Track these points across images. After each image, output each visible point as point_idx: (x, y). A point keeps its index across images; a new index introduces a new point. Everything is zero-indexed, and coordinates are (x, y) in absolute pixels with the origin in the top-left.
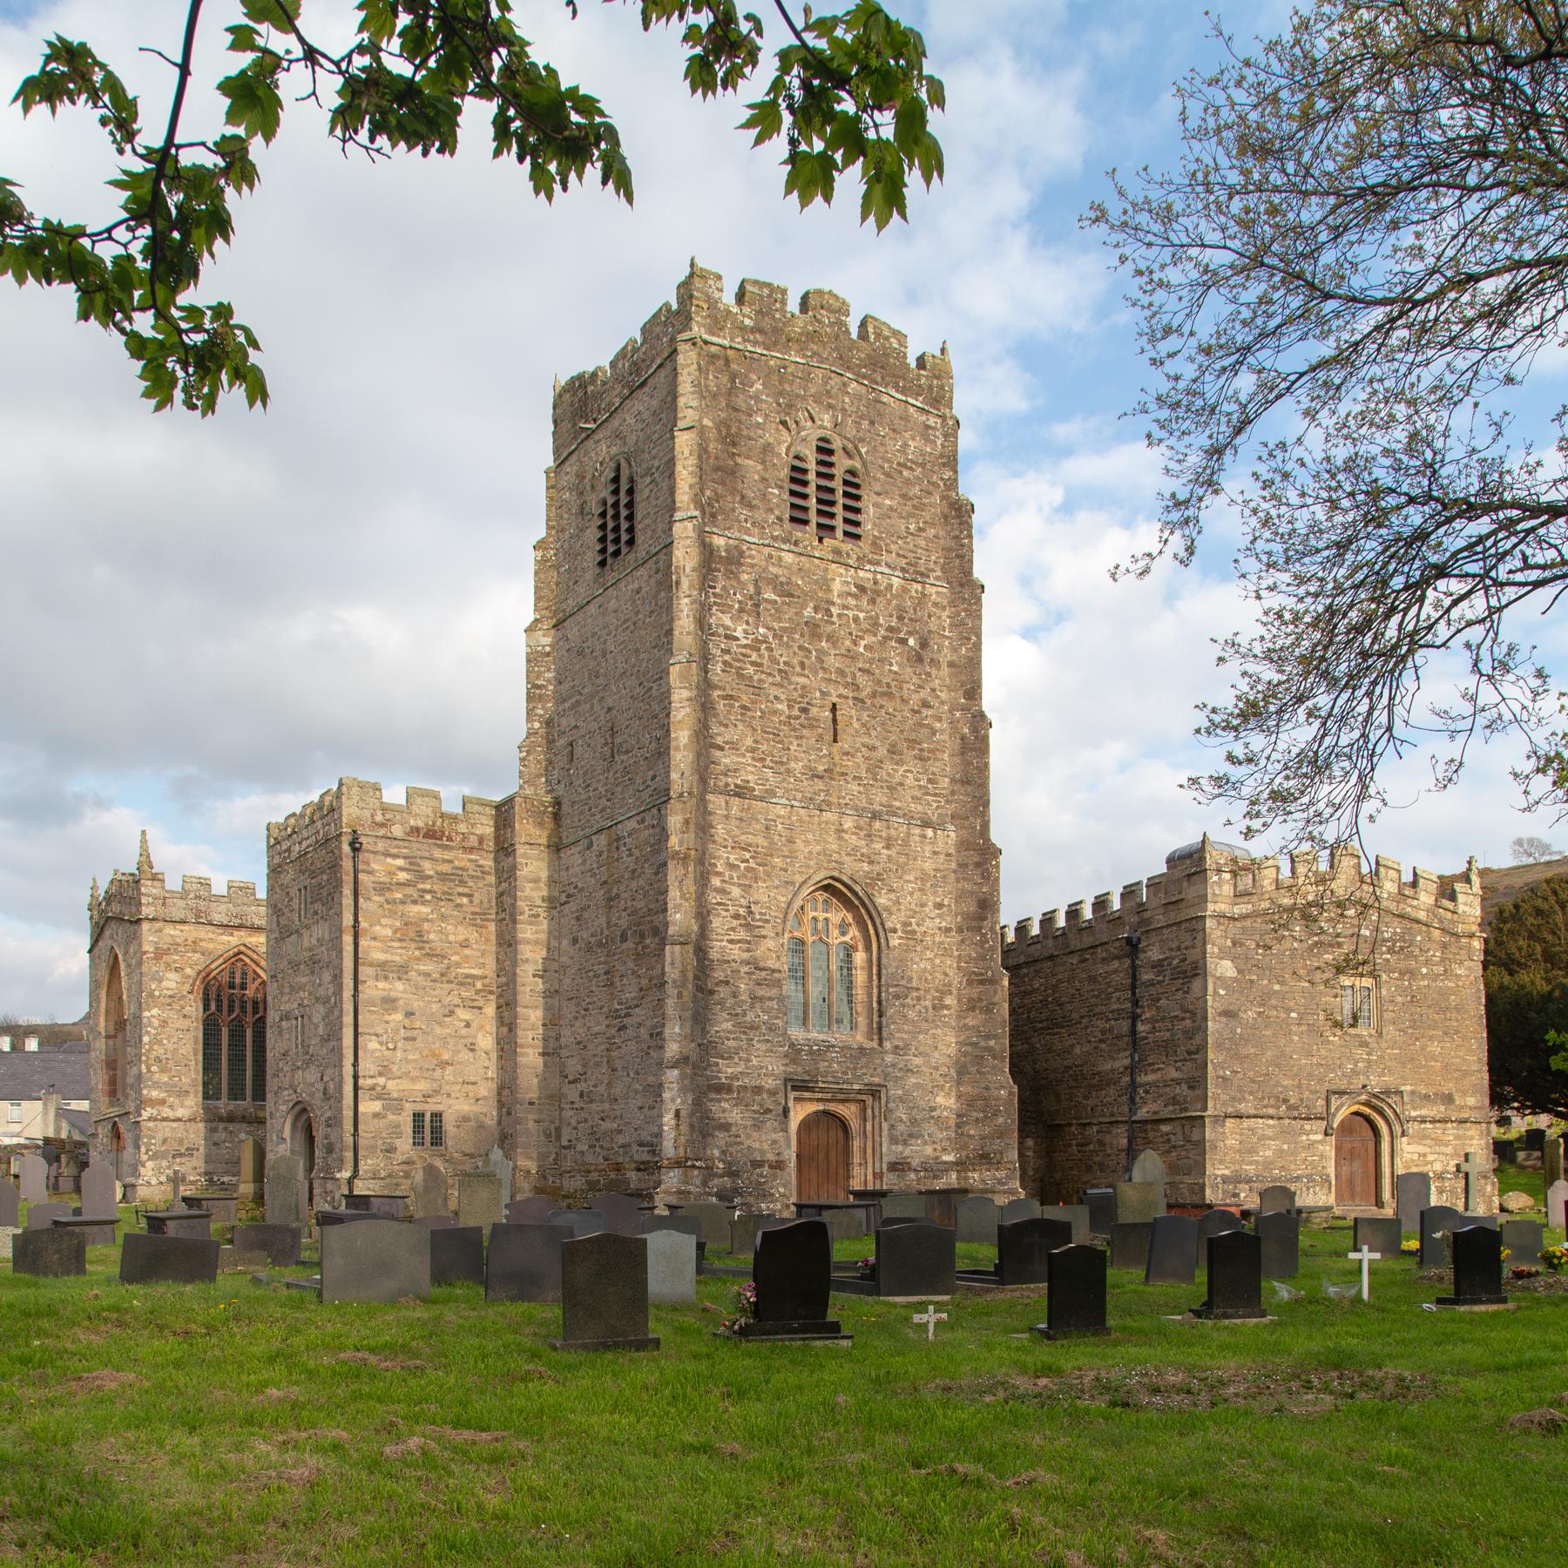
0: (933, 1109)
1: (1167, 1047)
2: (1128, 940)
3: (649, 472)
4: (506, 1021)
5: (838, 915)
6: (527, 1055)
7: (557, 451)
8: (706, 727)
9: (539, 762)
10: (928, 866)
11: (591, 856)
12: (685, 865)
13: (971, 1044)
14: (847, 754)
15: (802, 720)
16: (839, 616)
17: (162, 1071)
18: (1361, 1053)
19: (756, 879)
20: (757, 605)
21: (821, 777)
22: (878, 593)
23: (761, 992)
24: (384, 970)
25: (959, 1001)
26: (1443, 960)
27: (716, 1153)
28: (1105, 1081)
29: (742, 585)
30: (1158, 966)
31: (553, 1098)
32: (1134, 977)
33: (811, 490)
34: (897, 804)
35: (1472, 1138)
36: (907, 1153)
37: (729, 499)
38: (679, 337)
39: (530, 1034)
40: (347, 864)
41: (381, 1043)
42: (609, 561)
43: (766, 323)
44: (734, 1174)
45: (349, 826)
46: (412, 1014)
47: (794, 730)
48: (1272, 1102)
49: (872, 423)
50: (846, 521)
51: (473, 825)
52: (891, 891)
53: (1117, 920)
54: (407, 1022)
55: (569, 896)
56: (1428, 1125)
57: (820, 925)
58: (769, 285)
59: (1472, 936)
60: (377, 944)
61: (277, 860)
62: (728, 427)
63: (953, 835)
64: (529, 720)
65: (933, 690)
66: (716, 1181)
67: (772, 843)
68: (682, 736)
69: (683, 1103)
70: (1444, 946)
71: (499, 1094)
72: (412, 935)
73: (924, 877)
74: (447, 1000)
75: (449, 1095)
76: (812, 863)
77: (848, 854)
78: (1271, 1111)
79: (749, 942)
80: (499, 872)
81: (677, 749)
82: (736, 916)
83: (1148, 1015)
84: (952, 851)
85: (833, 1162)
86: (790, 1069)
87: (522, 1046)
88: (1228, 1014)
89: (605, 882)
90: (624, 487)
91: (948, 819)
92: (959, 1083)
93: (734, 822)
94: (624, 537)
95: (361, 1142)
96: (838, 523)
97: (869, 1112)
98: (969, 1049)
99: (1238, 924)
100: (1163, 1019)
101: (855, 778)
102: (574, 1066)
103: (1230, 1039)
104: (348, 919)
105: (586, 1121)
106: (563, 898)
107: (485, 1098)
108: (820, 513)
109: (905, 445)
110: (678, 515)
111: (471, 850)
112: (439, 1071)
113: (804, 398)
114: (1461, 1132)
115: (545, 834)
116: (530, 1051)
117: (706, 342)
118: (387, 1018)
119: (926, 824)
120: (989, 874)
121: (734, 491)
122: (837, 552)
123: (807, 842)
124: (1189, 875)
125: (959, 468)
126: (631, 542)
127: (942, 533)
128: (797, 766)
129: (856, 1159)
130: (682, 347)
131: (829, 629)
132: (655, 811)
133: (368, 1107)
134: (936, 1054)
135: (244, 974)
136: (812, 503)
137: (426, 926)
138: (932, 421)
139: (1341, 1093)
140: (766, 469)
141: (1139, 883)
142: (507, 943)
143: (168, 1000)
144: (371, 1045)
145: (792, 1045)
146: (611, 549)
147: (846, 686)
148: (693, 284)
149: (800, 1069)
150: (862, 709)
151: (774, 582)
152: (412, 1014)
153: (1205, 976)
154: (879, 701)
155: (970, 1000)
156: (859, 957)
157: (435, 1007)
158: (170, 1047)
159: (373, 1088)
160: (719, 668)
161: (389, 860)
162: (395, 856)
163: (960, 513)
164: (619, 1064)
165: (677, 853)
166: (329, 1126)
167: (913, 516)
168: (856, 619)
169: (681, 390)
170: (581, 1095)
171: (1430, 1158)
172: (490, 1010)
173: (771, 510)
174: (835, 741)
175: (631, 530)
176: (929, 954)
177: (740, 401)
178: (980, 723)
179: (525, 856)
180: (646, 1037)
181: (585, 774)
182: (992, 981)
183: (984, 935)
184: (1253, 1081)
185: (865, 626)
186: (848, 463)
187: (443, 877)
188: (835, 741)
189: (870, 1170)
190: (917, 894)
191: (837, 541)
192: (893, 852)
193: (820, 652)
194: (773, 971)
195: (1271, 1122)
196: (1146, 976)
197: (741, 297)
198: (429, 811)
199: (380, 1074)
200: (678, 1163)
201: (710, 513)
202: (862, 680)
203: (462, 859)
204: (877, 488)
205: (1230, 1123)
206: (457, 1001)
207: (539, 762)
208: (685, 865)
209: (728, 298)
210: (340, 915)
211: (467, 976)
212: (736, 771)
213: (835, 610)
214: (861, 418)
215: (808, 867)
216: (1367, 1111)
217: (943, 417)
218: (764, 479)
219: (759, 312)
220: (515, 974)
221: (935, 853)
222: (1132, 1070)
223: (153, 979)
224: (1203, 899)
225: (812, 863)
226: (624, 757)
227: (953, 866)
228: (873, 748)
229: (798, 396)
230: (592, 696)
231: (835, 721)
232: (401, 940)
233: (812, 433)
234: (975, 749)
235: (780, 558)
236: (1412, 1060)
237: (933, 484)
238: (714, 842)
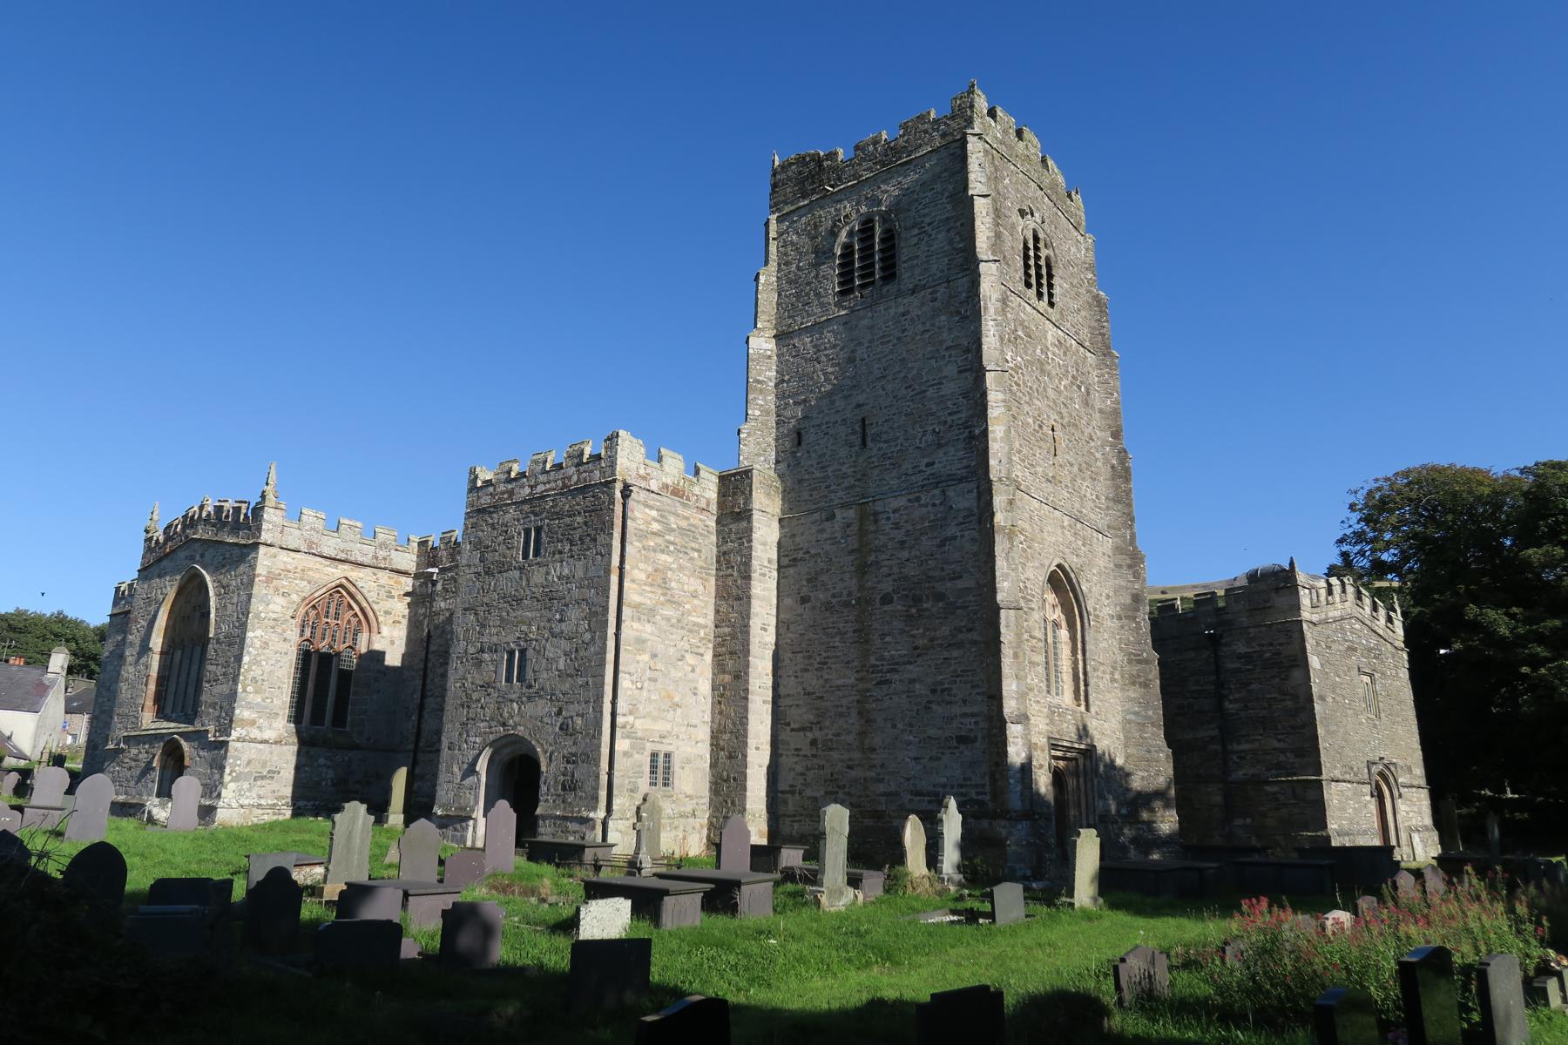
17: (256, 692)
25: (1122, 676)
30: (1247, 657)
41: (632, 682)
51: (704, 489)
60: (634, 586)
72: (660, 581)
81: (995, 440)
98: (1132, 717)
107: (702, 741)
118: (638, 658)
130: (970, 139)
143: (272, 623)
155: (1132, 676)
157: (672, 650)
158: (267, 668)
161: (647, 510)
162: (651, 508)
172: (709, 657)
183: (1138, 623)
195: (1349, 785)
199: (631, 713)
206: (687, 647)
211: (696, 624)
213: (1050, 356)
223: (262, 601)
232: (652, 585)
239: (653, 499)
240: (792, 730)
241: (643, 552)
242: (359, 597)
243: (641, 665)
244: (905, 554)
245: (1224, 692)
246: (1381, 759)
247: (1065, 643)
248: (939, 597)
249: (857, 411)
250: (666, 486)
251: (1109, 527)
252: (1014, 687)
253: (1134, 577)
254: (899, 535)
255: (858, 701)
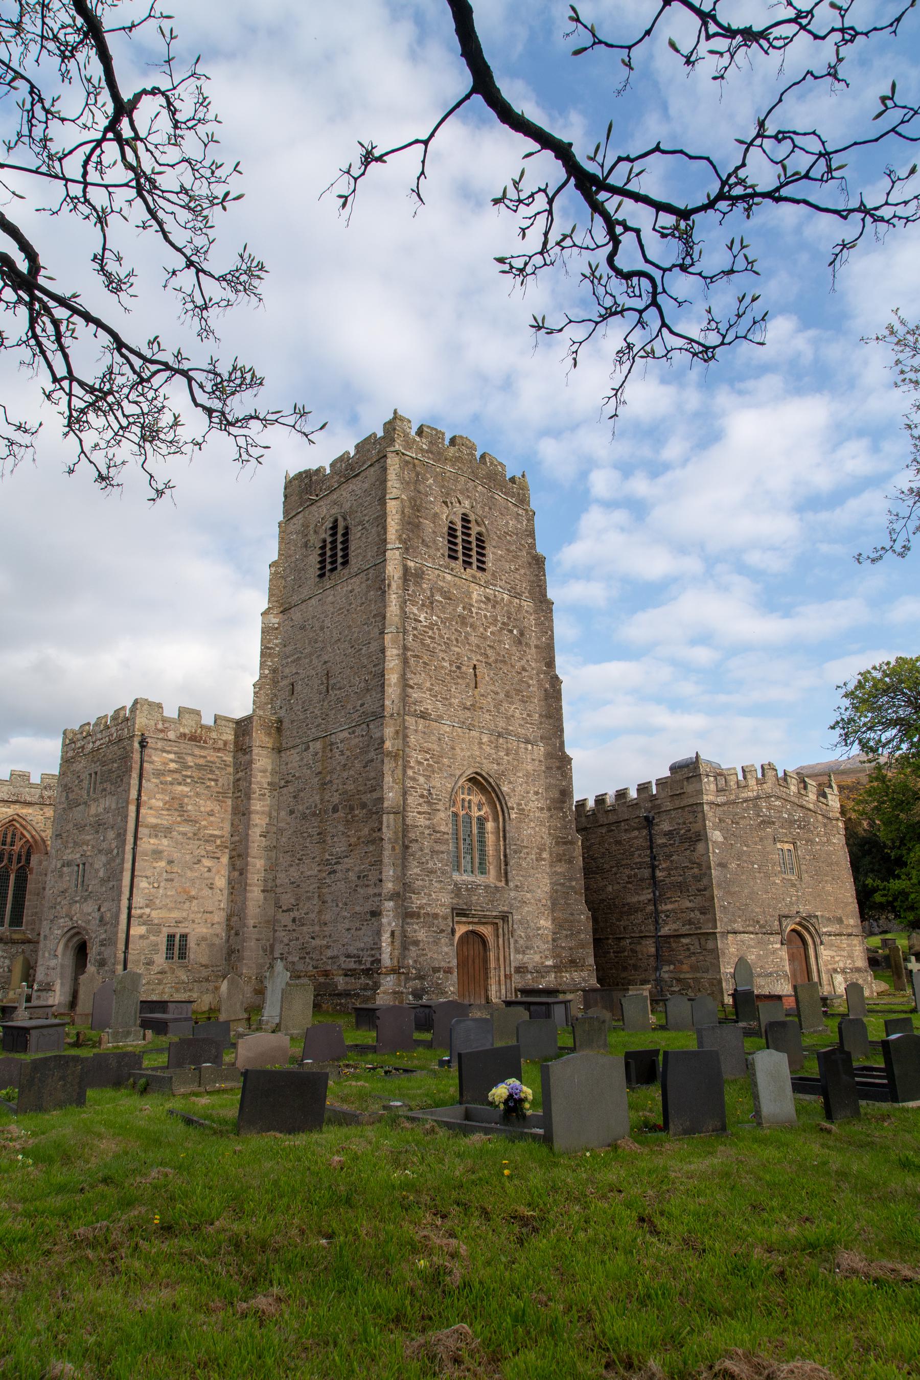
0: (539, 929)
1: (681, 887)
2: (646, 818)
3: (361, 523)
4: (237, 867)
5: (476, 798)
6: (254, 891)
7: (286, 512)
8: (405, 674)
9: (267, 695)
10: (530, 767)
11: (308, 756)
12: (396, 761)
13: (560, 884)
14: (483, 695)
15: (458, 673)
16: (477, 613)
18: (792, 891)
19: (433, 772)
20: (432, 603)
21: (469, 709)
22: (497, 602)
23: (437, 847)
24: (156, 830)
25: (551, 855)
26: (826, 833)
27: (411, 962)
28: (634, 909)
29: (424, 591)
30: (669, 834)
31: (272, 923)
32: (651, 841)
33: (459, 541)
34: (511, 728)
35: (855, 946)
36: (525, 960)
37: (416, 540)
38: (388, 449)
39: (256, 877)
40: (136, 756)
41: (149, 883)
42: (327, 574)
43: (434, 448)
44: (421, 978)
45: (139, 730)
46: (172, 862)
47: (453, 679)
48: (751, 923)
49: (490, 509)
50: (478, 560)
51: (221, 734)
52: (510, 783)
53: (635, 805)
54: (168, 868)
55: (287, 782)
56: (833, 938)
57: (466, 804)
58: (436, 429)
59: (837, 819)
60: (152, 812)
61: (71, 754)
62: (416, 501)
63: (542, 749)
64: (261, 668)
65: (528, 661)
66: (411, 983)
67: (442, 749)
68: (392, 678)
69: (396, 925)
70: (825, 825)
71: (228, 920)
72: (177, 806)
73: (527, 775)
74: (196, 853)
75: (193, 921)
76: (465, 763)
77: (485, 758)
78: (751, 929)
79: (429, 814)
80: (238, 767)
81: (390, 685)
82: (422, 796)
83: (664, 866)
84: (542, 759)
85: (477, 968)
86: (455, 901)
87: (250, 885)
88: (723, 865)
89: (320, 773)
90: (340, 531)
91: (539, 739)
92: (553, 911)
93: (421, 735)
94: (340, 560)
95: (130, 957)
96: (474, 560)
97: (501, 931)
98: (559, 887)
99: (721, 809)
100: (676, 868)
101: (488, 711)
102: (287, 899)
103: (724, 881)
104: (134, 794)
105: (297, 939)
106: (282, 783)
107: (218, 923)
108: (464, 554)
109: (507, 523)
110: (389, 546)
111: (219, 750)
112: (188, 904)
113: (455, 491)
114: (849, 942)
115: (271, 741)
116: (256, 889)
117: (403, 454)
118: (155, 864)
119: (527, 742)
120: (566, 774)
121: (419, 537)
122: (474, 577)
123: (462, 749)
124: (688, 778)
125: (536, 537)
126: (345, 563)
127: (528, 573)
128: (455, 701)
129: (493, 965)
130: (389, 455)
131: (471, 620)
132: (364, 726)
133: (137, 930)
134: (539, 891)
135: (14, 835)
136: (460, 548)
137: (186, 800)
138: (520, 512)
139: (786, 917)
140: (435, 526)
141: (650, 782)
142: (241, 813)
144: (142, 884)
145: (456, 885)
146: (329, 567)
147: (481, 654)
148: (393, 425)
149: (461, 901)
150: (491, 669)
151: (441, 590)
152: (172, 862)
153: (707, 840)
154: (499, 665)
156: (490, 826)
157: (188, 857)
159: (141, 917)
160: (411, 638)
161: (165, 754)
162: (169, 752)
163: (538, 563)
164: (329, 898)
165: (391, 752)
166: (102, 945)
167: (513, 561)
168: (485, 616)
169: (389, 477)
170: (294, 920)
171: (837, 959)
172: (225, 860)
173: (438, 550)
174: (476, 687)
175: (345, 556)
176: (532, 824)
177: (421, 488)
178: (555, 681)
179: (259, 755)
180: (354, 878)
181: (304, 702)
182: (572, 843)
184: (740, 909)
185: (490, 620)
186: (478, 529)
187: (199, 767)
188: (476, 687)
189: (502, 973)
190: (524, 786)
191: (472, 571)
192: (510, 758)
193: (467, 633)
194: (444, 833)
195: (752, 936)
196: (661, 841)
197: (420, 432)
198: (193, 723)
199: (147, 906)
200: (394, 971)
201: (407, 549)
202: (490, 652)
203: (212, 756)
204: (494, 543)
205: (730, 936)
206: (203, 853)
207: (267, 695)
208: (396, 761)
209: (413, 432)
210: (128, 791)
211: (211, 836)
212: (421, 702)
213: (474, 610)
214: (485, 505)
215: (463, 765)
216: (800, 928)
217: (526, 510)
218: (434, 532)
219: (431, 442)
220: (247, 835)
221: (533, 760)
222: (655, 902)
224: (700, 792)
225: (465, 763)
226: (338, 692)
227: (543, 768)
228: (497, 693)
229: (452, 489)
230: (311, 654)
231: (475, 675)
232: (168, 810)
233: (459, 510)
234: (553, 697)
235: (444, 577)
236: (819, 895)
237: (522, 545)
238: (409, 747)
239: (171, 746)
240: (283, 911)
241: (160, 786)
242: (29, 827)
243: (158, 870)
244: (345, 774)
245: (656, 863)
246: (798, 912)
247: (492, 833)
248: (364, 806)
249: (324, 667)
250: (183, 735)
251: (541, 738)
252: (391, 873)
253: (562, 776)
254: (342, 759)
255: (319, 888)
